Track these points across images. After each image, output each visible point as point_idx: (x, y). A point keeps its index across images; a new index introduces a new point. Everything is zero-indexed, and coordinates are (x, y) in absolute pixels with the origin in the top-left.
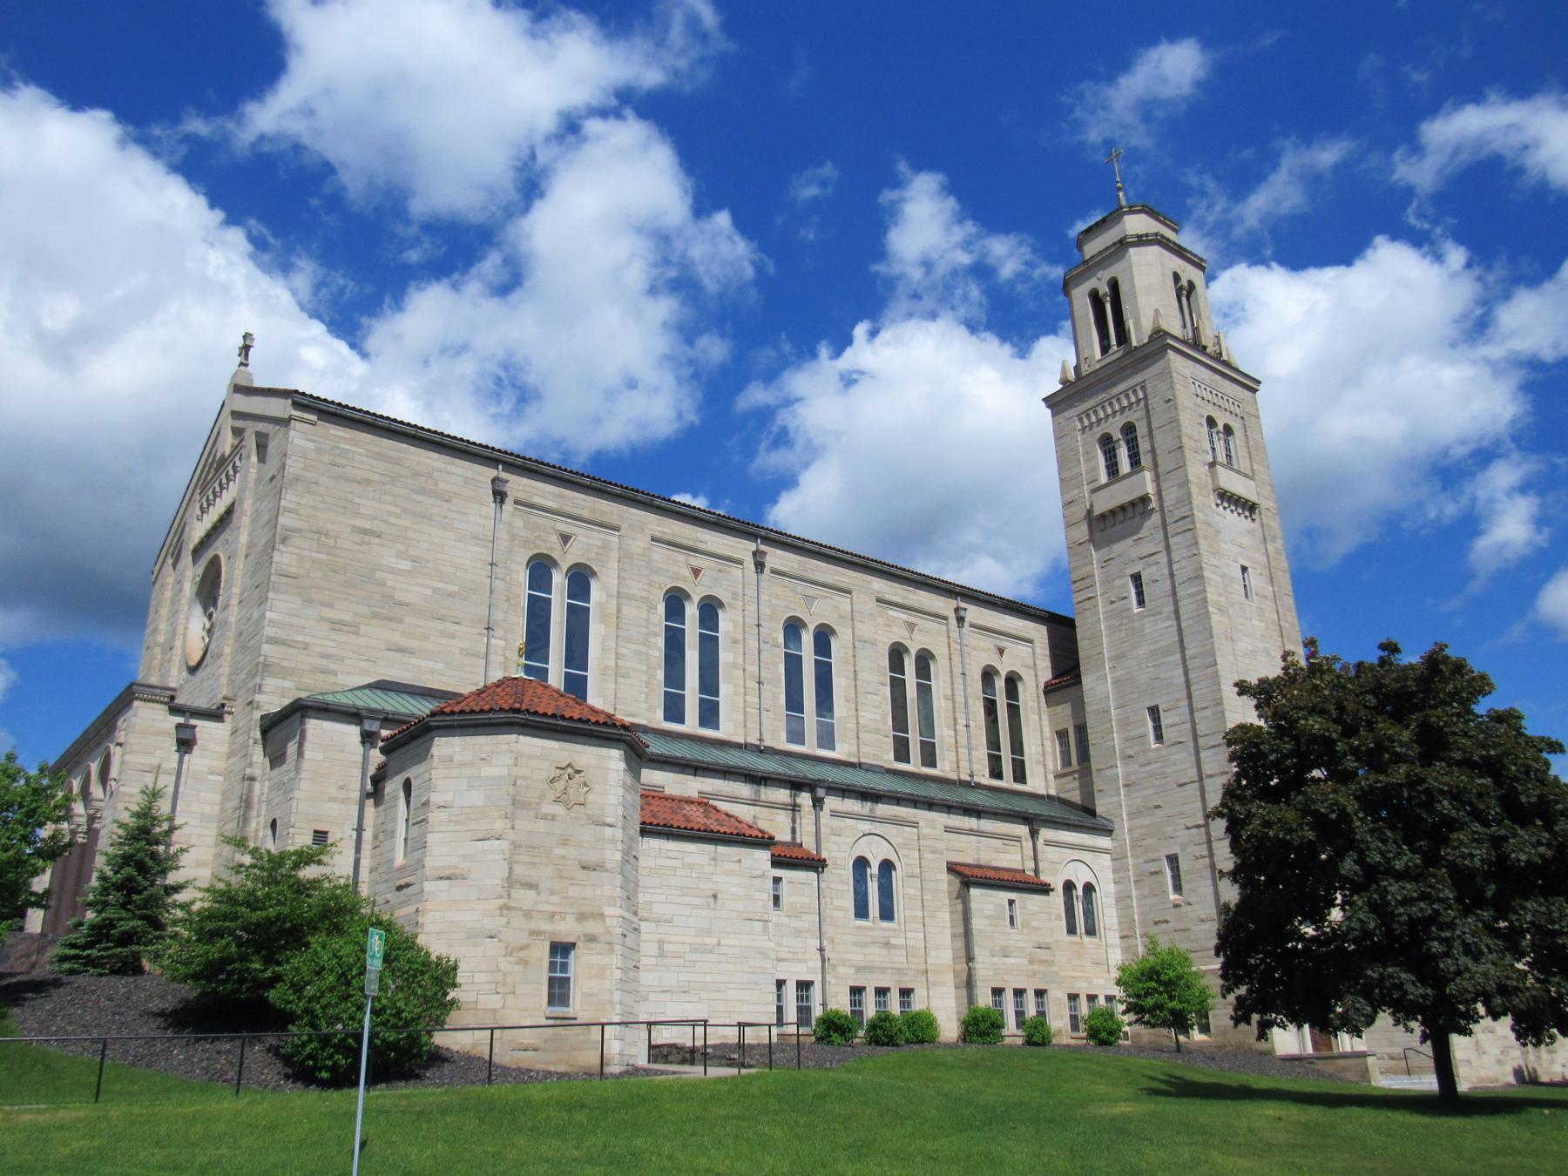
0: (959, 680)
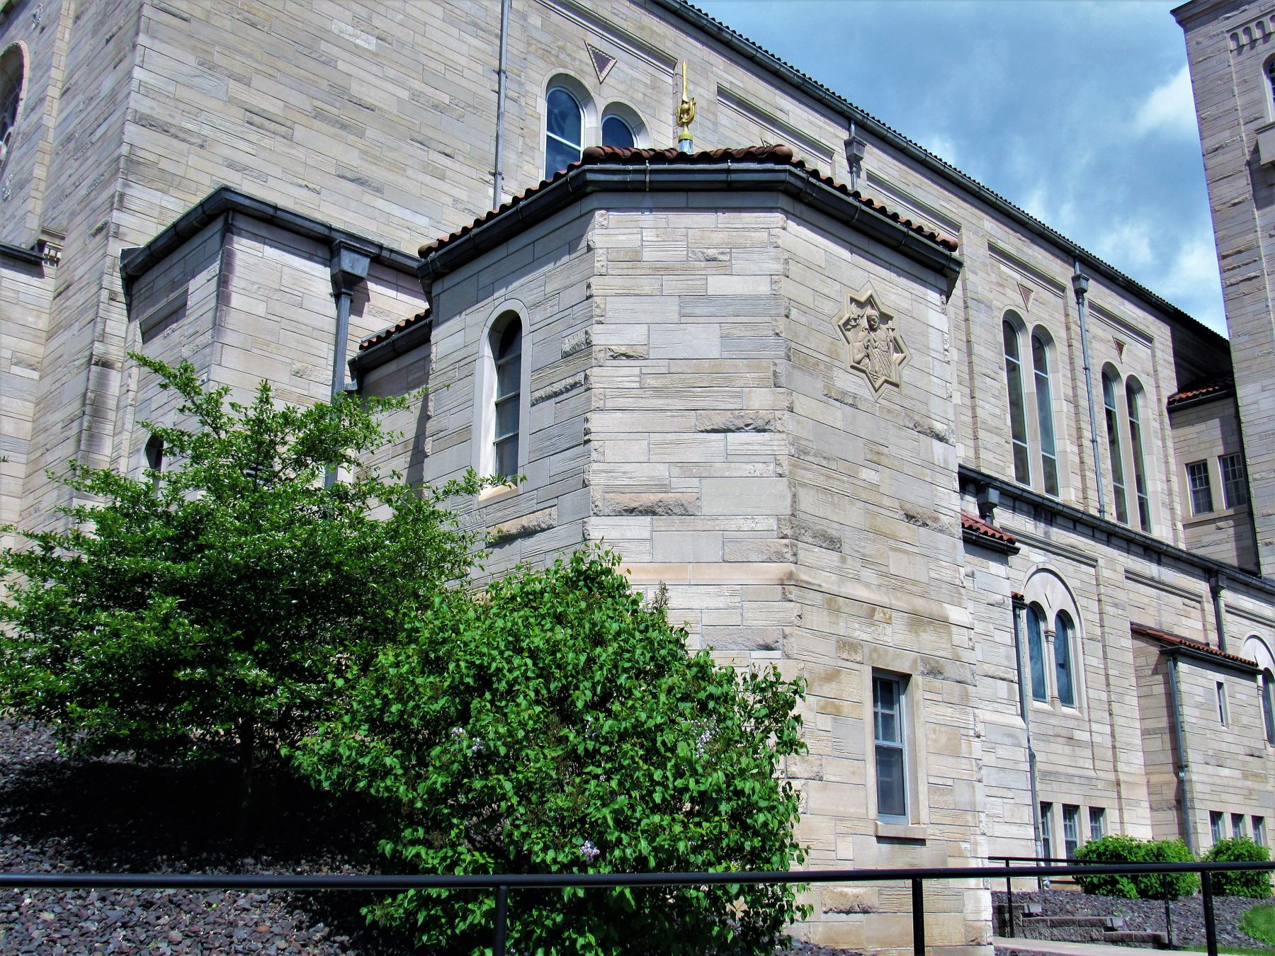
0: (1081, 375)
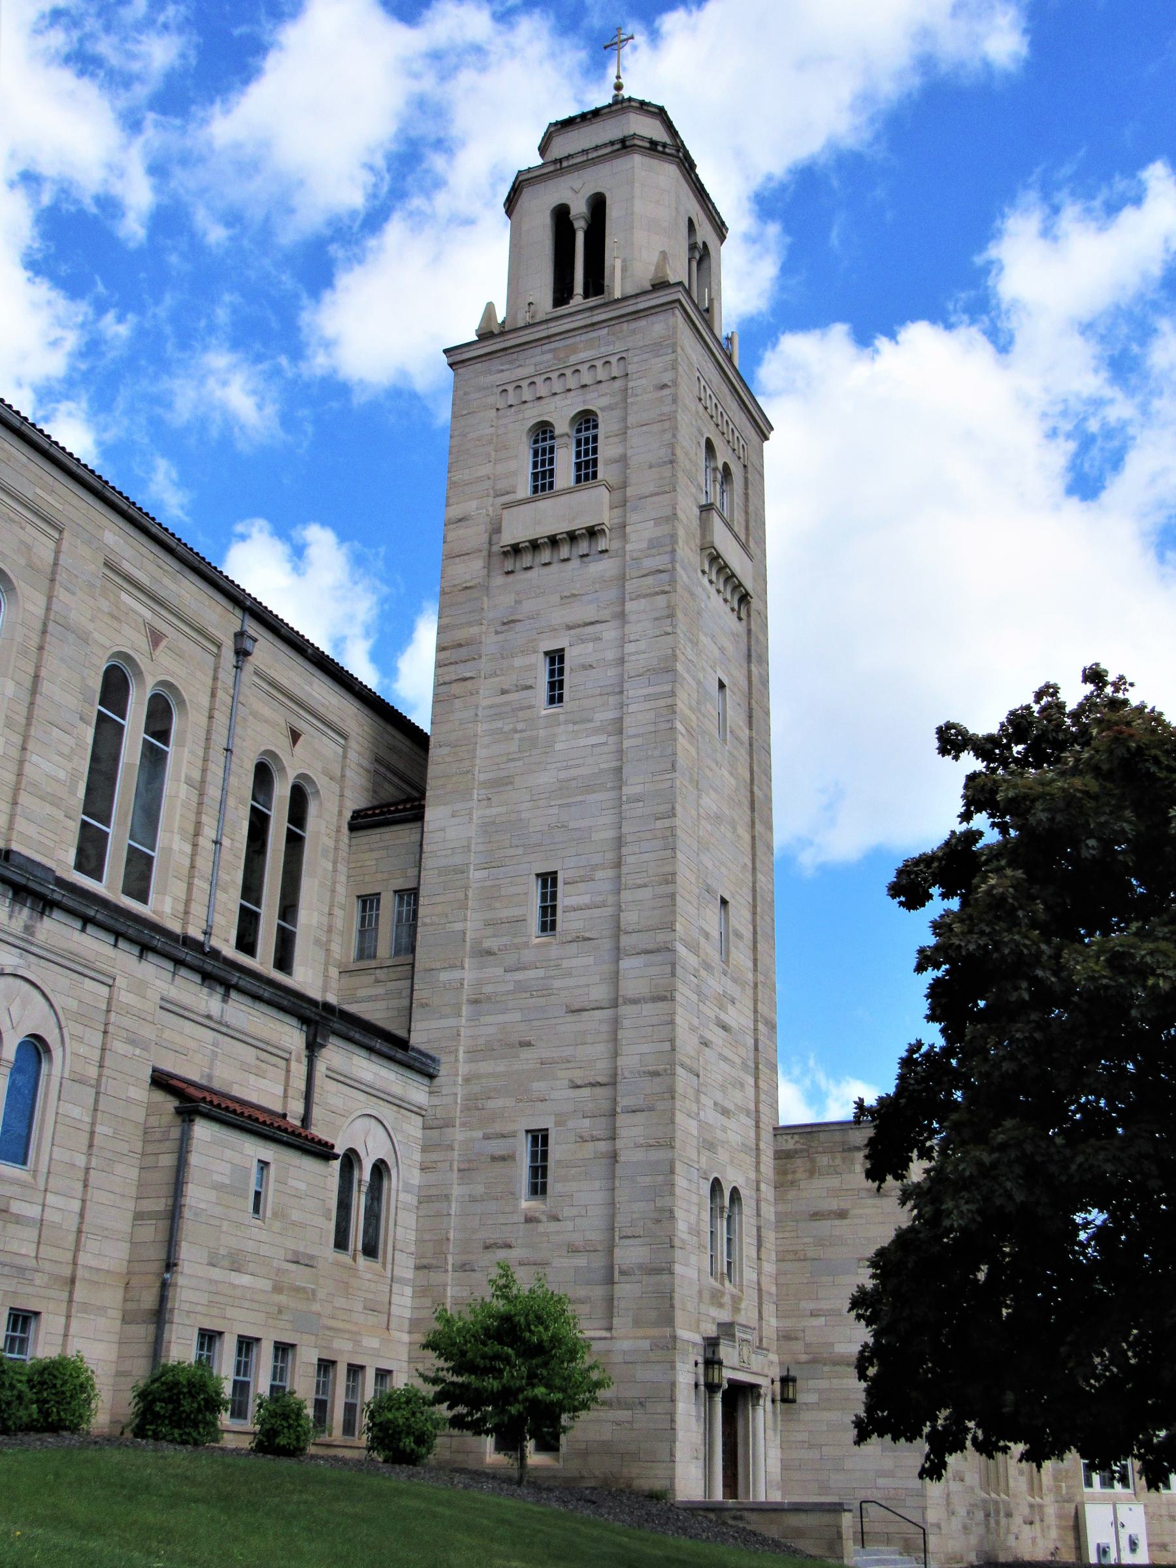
0: (218, 756)
